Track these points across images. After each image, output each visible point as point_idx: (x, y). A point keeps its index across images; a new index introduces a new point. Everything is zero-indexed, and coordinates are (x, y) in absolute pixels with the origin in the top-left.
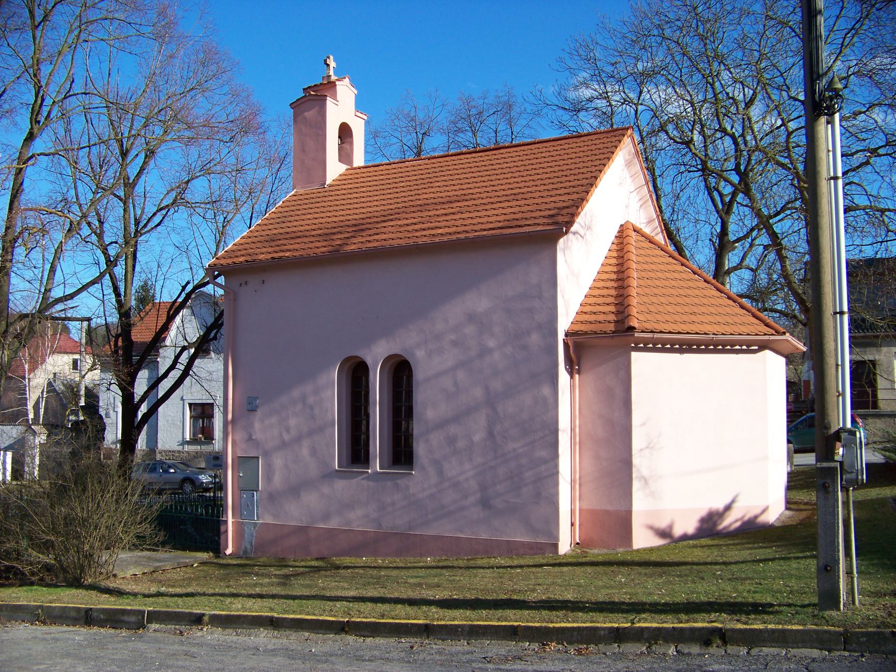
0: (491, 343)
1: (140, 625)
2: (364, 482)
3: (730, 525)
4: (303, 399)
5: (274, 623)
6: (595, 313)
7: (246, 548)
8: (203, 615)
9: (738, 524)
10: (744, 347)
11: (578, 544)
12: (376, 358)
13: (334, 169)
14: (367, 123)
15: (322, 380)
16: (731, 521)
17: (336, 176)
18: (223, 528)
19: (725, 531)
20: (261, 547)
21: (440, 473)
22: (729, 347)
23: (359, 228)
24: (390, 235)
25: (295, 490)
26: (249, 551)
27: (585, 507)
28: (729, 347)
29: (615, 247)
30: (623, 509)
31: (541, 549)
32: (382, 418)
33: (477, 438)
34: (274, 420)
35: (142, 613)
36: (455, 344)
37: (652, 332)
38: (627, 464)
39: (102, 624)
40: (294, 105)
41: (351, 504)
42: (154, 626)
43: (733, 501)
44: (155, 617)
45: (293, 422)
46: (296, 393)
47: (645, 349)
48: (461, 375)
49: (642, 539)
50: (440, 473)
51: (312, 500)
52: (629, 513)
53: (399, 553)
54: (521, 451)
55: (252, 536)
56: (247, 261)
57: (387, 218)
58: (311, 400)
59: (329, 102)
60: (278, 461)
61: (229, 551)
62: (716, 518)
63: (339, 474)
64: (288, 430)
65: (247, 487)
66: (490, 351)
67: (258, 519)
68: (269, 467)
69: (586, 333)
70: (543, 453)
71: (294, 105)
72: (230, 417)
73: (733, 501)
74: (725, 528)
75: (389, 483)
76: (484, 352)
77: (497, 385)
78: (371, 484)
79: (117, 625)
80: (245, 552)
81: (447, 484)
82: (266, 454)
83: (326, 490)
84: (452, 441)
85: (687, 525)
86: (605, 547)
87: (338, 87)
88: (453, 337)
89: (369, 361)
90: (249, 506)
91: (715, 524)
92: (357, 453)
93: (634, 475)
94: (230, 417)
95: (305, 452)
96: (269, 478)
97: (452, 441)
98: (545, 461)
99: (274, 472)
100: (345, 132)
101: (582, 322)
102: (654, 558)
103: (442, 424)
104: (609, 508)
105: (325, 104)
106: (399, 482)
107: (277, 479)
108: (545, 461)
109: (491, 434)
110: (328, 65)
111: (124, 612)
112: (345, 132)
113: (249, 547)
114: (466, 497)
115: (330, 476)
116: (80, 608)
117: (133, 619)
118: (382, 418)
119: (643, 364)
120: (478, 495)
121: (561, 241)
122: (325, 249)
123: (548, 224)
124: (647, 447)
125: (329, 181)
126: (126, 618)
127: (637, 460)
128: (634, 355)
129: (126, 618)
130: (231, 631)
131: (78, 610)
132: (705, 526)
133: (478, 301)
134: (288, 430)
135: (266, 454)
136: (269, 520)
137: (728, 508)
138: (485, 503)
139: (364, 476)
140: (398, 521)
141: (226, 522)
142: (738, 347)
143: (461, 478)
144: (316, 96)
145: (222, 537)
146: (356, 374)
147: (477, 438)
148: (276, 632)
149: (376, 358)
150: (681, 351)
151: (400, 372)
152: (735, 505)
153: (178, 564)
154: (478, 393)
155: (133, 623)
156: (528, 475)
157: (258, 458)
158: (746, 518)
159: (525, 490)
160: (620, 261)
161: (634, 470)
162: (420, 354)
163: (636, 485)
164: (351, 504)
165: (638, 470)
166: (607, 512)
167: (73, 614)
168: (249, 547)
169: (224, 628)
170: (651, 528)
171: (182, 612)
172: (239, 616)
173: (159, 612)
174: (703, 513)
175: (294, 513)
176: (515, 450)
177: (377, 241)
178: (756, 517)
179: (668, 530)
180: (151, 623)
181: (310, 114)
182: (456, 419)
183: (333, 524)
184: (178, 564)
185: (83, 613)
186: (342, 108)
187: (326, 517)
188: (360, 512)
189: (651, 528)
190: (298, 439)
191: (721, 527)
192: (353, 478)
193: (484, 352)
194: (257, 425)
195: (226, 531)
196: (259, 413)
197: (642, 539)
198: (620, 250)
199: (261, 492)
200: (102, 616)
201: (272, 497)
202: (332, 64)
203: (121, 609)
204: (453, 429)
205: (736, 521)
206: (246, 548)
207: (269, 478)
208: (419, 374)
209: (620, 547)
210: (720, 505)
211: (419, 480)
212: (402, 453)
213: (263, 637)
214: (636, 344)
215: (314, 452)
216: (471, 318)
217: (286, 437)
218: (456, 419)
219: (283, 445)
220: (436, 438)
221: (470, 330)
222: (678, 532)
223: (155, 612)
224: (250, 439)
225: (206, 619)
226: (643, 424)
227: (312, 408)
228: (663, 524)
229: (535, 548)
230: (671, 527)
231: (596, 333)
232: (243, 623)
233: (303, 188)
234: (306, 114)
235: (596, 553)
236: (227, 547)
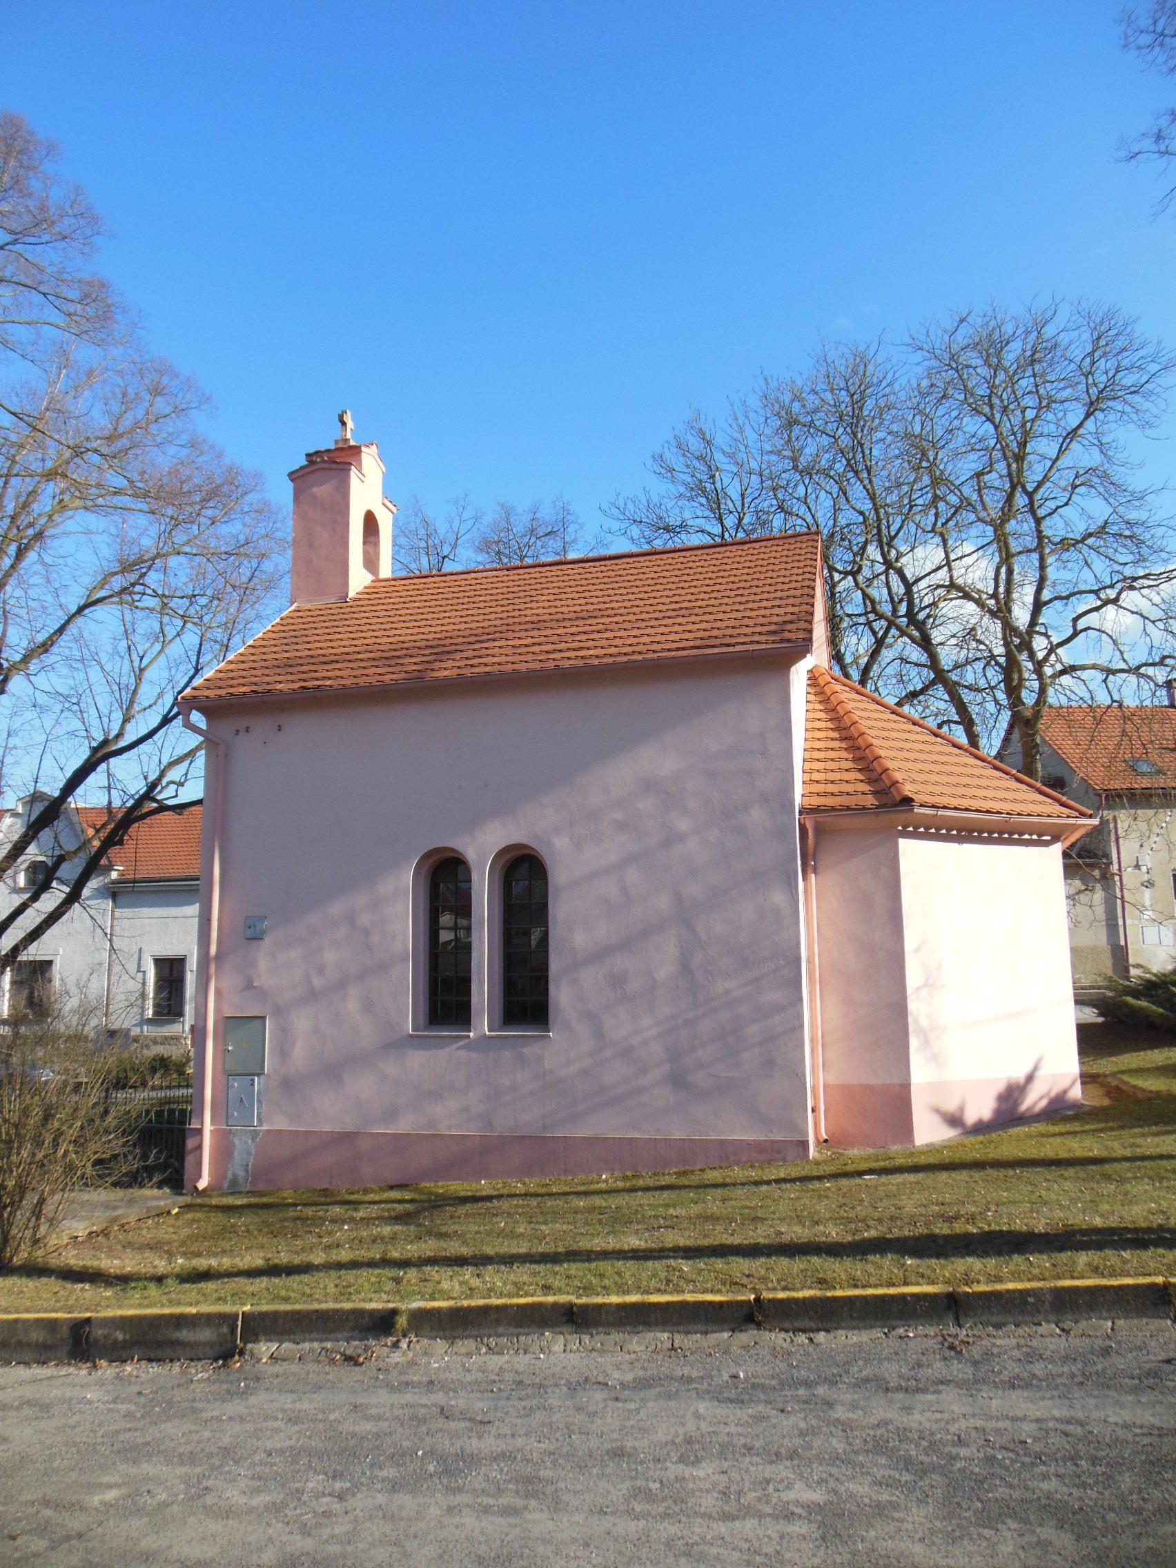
0: (684, 825)
1: (225, 1353)
2: (463, 1053)
3: (1035, 1104)
4: (351, 918)
5: (575, 1319)
6: (832, 782)
7: (235, 1177)
8: (394, 1312)
9: (1043, 1103)
10: (1035, 837)
11: (826, 1141)
12: (481, 851)
13: (358, 580)
14: (395, 520)
15: (386, 886)
16: (1034, 1099)
17: (360, 589)
18: (190, 1143)
19: (1028, 1114)
20: (265, 1171)
21: (599, 1034)
22: (1016, 836)
23: (440, 650)
24: (498, 658)
25: (331, 1071)
26: (241, 1180)
27: (832, 1080)
28: (1016, 836)
29: (812, 698)
30: (896, 1081)
31: (779, 1151)
32: (491, 950)
33: (661, 975)
34: (295, 954)
35: (229, 1319)
36: (621, 826)
37: (933, 806)
38: (899, 1010)
39: (118, 1353)
40: (295, 476)
41: (452, 1091)
42: (265, 1348)
43: (1036, 1068)
44: (260, 1326)
45: (330, 957)
46: (337, 908)
47: (915, 835)
48: (632, 875)
49: (928, 1132)
50: (599, 1034)
51: (364, 1086)
52: (906, 1087)
53: (526, 1170)
54: (738, 993)
55: (249, 1153)
56: (232, 695)
57: (482, 637)
58: (365, 919)
59: (354, 472)
60: (301, 1023)
61: (202, 1184)
62: (1016, 1095)
63: (414, 1041)
64: (321, 970)
65: (242, 1069)
66: (682, 837)
67: (260, 1123)
68: (284, 1034)
69: (833, 809)
70: (775, 996)
71: (295, 476)
72: (213, 949)
73: (1036, 1068)
74: (1028, 1109)
75: (507, 1054)
76: (672, 839)
77: (693, 890)
78: (473, 1055)
79: (160, 1354)
80: (234, 1182)
81: (609, 1052)
82: (279, 1011)
83: (391, 1068)
84: (618, 981)
85: (981, 1109)
86: (868, 1145)
87: (364, 456)
88: (618, 816)
89: (471, 854)
90: (244, 1102)
91: (1017, 1103)
92: (446, 1002)
93: (911, 1029)
94: (213, 949)
95: (352, 1005)
96: (283, 1052)
97: (618, 981)
98: (780, 1009)
99: (298, 1039)
100: (370, 522)
101: (818, 794)
102: (946, 1156)
103: (602, 953)
104: (872, 1081)
105: (348, 477)
106: (525, 1050)
107: (299, 1053)
108: (780, 1009)
109: (685, 968)
110: (344, 423)
111: (180, 1321)
112: (370, 522)
113: (241, 1174)
114: (644, 1071)
115: (397, 1045)
116: (56, 1321)
117: (205, 1335)
118: (491, 950)
119: (918, 858)
120: (667, 1067)
121: (793, 669)
122: (394, 677)
123: (773, 642)
124: (925, 985)
125: (351, 594)
126: (185, 1335)
127: (914, 1005)
128: (903, 843)
129: (185, 1335)
130: (470, 1344)
131: (52, 1325)
132: (1004, 1107)
133: (661, 759)
134: (321, 970)
135: (279, 1011)
136: (281, 1123)
137: (1030, 1078)
138: (678, 1081)
139: (461, 1043)
140: (524, 1116)
141: (199, 1132)
142: (1026, 837)
143: (635, 1041)
144: (329, 466)
145: (189, 1160)
146: (444, 877)
147: (661, 975)
148: (586, 1338)
149: (481, 851)
150: (959, 839)
151: (524, 872)
152: (1041, 1073)
153: (148, 1210)
154: (663, 903)
155: (205, 1344)
156: (752, 1030)
157: (264, 1018)
158: (1053, 1094)
159: (746, 1056)
160: (833, 715)
161: (910, 1019)
162: (561, 843)
163: (914, 1043)
164: (452, 1091)
165: (916, 1021)
166: (869, 1088)
167: (37, 1336)
168: (241, 1174)
169: (452, 1339)
170: (938, 1111)
171: (335, 1311)
172: (486, 1310)
173: (275, 1313)
174: (1000, 1087)
175: (329, 1112)
176: (727, 992)
177: (486, 665)
178: (1065, 1092)
179: (958, 1115)
180: (256, 1341)
181: (323, 490)
182: (625, 945)
183: (405, 1125)
184: (148, 1210)
185: (65, 1331)
186: (366, 490)
187: (391, 1114)
188: (453, 1104)
189: (938, 1111)
190: (341, 985)
191: (1023, 1107)
192: (437, 1048)
193: (672, 839)
194: (263, 963)
195: (200, 1147)
196: (268, 941)
197: (928, 1132)
198: (826, 701)
199: (268, 1075)
200: (120, 1336)
201: (288, 1085)
202: (350, 425)
203: (172, 1316)
204: (621, 962)
205: (1042, 1098)
206: (235, 1177)
207: (283, 1052)
208: (559, 876)
209: (894, 1143)
210: (1019, 1074)
211: (561, 1048)
212: (527, 1003)
213: (560, 1352)
214: (905, 827)
215: (368, 1005)
216: (649, 785)
217: (317, 982)
218: (625, 945)
219: (312, 995)
220: (590, 977)
221: (646, 805)
222: (971, 1118)
223: (263, 1315)
224: (249, 986)
225: (402, 1321)
226: (918, 949)
227: (366, 932)
228: (951, 1106)
229: (770, 1152)
230: (961, 1109)
231: (848, 808)
232: (498, 1322)
233: (309, 601)
234: (315, 489)
235: (856, 1154)
236: (200, 1176)
